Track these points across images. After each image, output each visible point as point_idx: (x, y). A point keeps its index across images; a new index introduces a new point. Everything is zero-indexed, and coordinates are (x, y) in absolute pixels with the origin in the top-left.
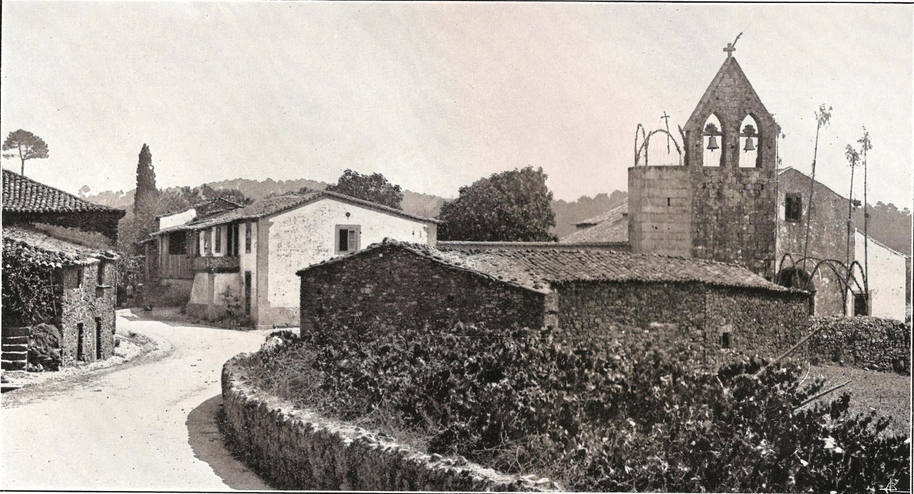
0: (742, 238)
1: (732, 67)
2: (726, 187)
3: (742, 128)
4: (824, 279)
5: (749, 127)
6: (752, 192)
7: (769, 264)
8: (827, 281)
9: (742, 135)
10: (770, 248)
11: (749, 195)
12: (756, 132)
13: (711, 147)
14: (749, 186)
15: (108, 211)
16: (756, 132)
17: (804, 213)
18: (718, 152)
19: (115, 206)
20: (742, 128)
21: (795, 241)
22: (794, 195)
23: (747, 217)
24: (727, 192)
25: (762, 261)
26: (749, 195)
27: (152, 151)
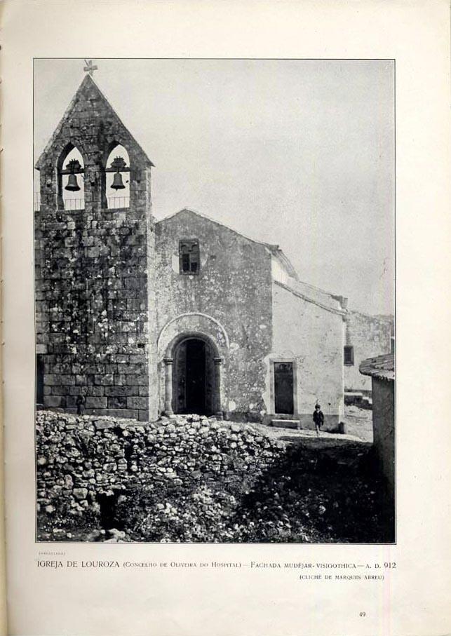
0: (108, 295)
1: (89, 95)
2: (85, 233)
3: (66, 162)
4: (232, 345)
5: (74, 163)
6: (117, 238)
7: (142, 327)
8: (237, 346)
9: (110, 171)
10: (142, 307)
11: (114, 242)
12: (128, 165)
13: (118, 186)
14: (114, 231)
15: (292, 382)
16: (128, 165)
17: (203, 263)
18: (126, 192)
19: (290, 361)
20: (66, 162)
21: (193, 299)
22: (189, 242)
23: (112, 269)
24: (88, 240)
25: (132, 324)
26: (114, 242)
27: (124, 189)
